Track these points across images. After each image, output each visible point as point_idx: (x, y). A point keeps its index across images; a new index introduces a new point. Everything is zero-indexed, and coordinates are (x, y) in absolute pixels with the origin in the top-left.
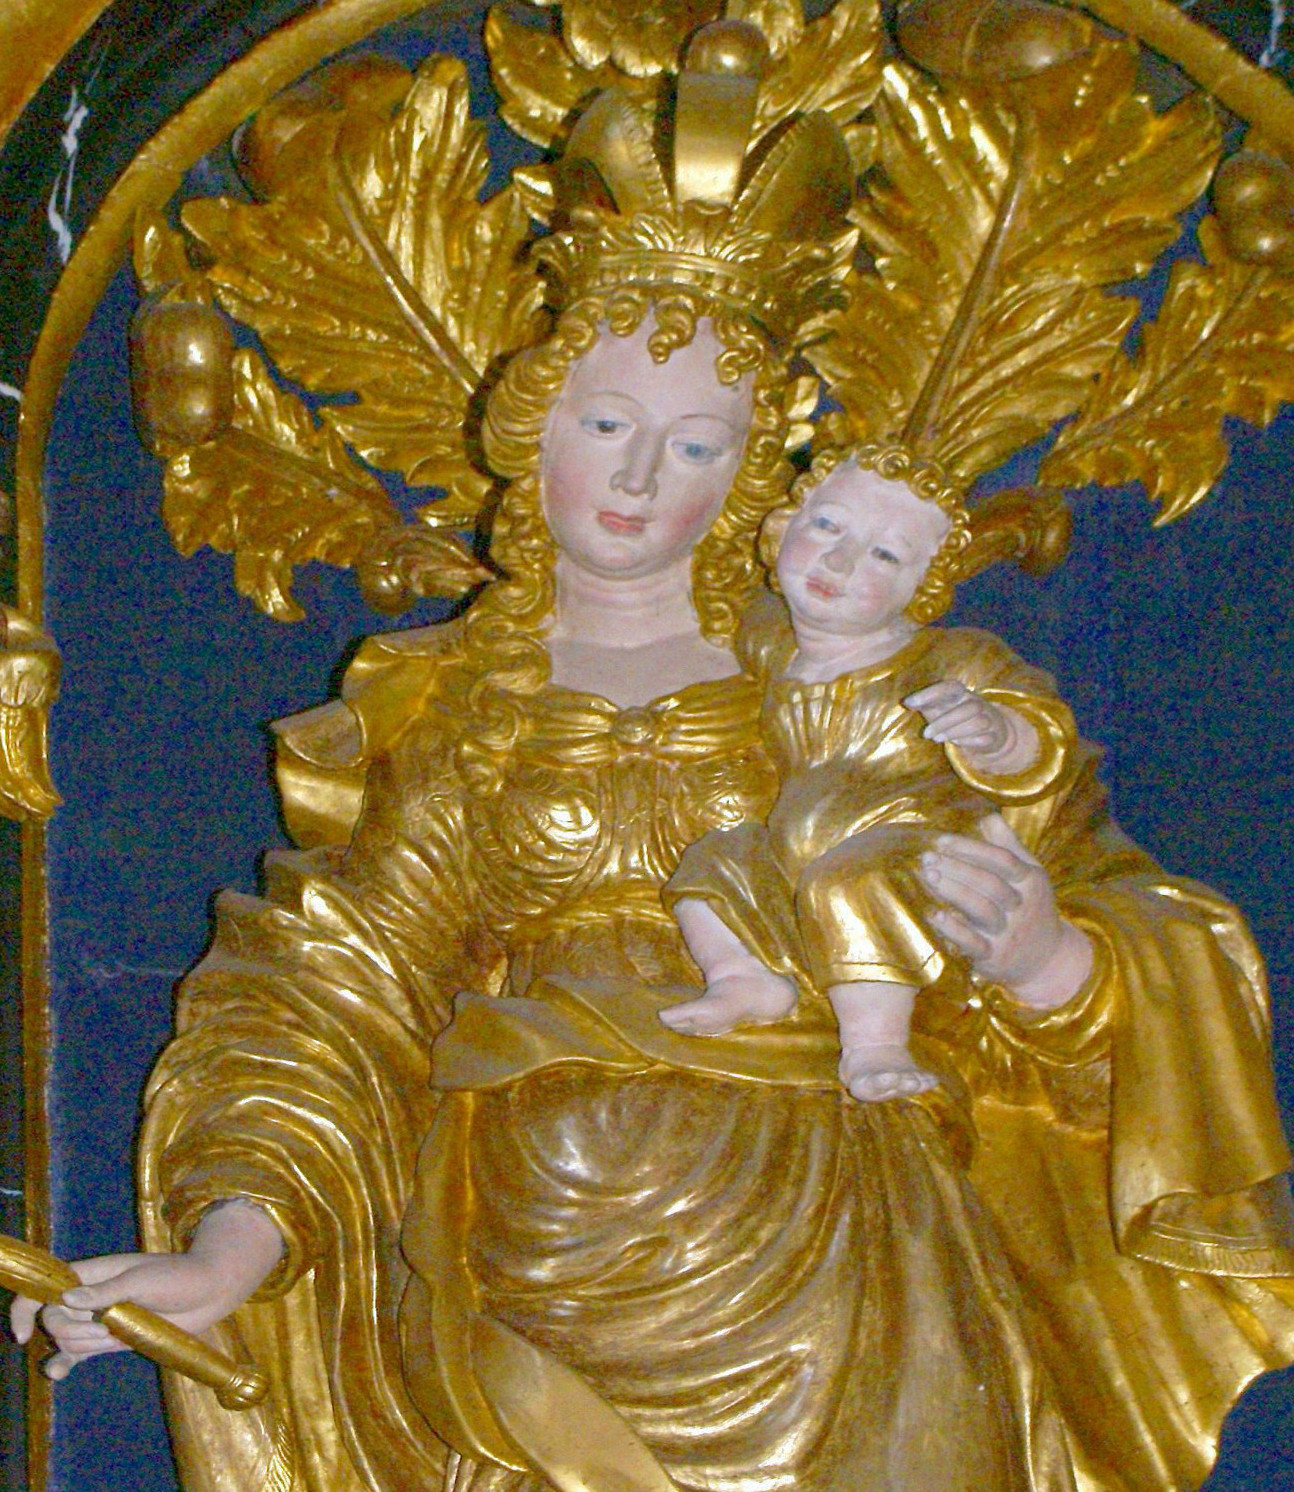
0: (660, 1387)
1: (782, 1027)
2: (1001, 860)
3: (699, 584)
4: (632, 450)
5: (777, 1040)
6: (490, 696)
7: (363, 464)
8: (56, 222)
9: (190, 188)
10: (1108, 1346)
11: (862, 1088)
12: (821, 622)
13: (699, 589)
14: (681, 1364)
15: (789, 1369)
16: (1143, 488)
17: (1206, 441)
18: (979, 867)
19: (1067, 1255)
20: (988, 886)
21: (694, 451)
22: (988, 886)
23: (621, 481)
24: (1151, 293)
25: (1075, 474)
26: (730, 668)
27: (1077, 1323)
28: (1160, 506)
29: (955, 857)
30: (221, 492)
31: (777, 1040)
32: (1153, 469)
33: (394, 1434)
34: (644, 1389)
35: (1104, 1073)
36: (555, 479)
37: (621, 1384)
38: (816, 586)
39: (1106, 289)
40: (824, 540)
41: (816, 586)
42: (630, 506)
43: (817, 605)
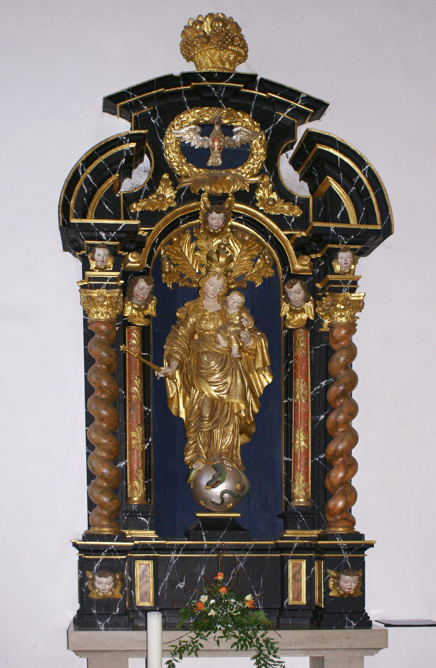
0: (215, 384)
1: (226, 348)
2: (247, 333)
3: (218, 299)
4: (214, 288)
5: (226, 349)
6: (199, 309)
7: (179, 272)
8: (154, 249)
9: (166, 244)
10: (253, 381)
11: (234, 356)
12: (232, 308)
13: (218, 300)
14: (216, 382)
15: (226, 383)
16: (254, 282)
17: (261, 279)
18: (245, 334)
19: (250, 371)
20: (246, 336)
21: (220, 288)
22: (246, 336)
23: (213, 291)
24: (255, 261)
25: (247, 279)
26: (220, 308)
27: (251, 378)
28: (257, 284)
29: (243, 333)
30: (167, 277)
31: (226, 349)
32: (255, 280)
33: (186, 384)
34: (213, 384)
35: (254, 352)
36: (206, 289)
37: (211, 384)
38: (231, 305)
39: (251, 260)
40: (232, 301)
41: (231, 305)
42: (213, 293)
43: (231, 306)
